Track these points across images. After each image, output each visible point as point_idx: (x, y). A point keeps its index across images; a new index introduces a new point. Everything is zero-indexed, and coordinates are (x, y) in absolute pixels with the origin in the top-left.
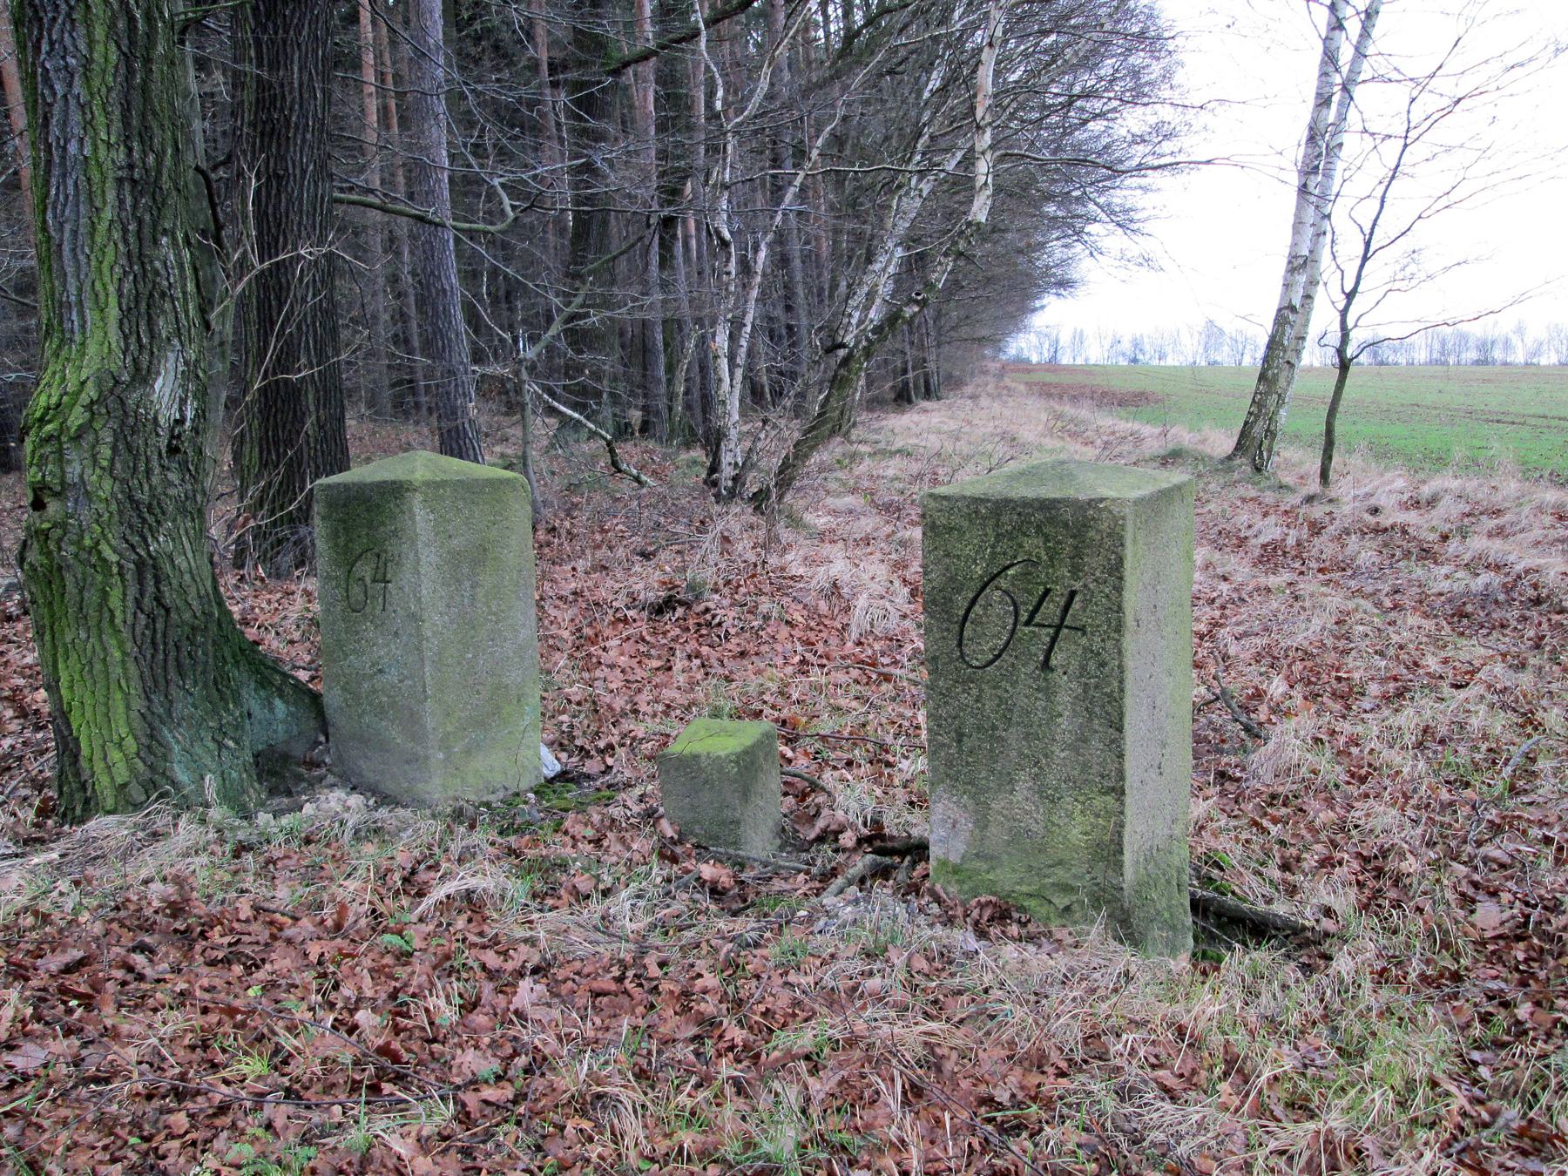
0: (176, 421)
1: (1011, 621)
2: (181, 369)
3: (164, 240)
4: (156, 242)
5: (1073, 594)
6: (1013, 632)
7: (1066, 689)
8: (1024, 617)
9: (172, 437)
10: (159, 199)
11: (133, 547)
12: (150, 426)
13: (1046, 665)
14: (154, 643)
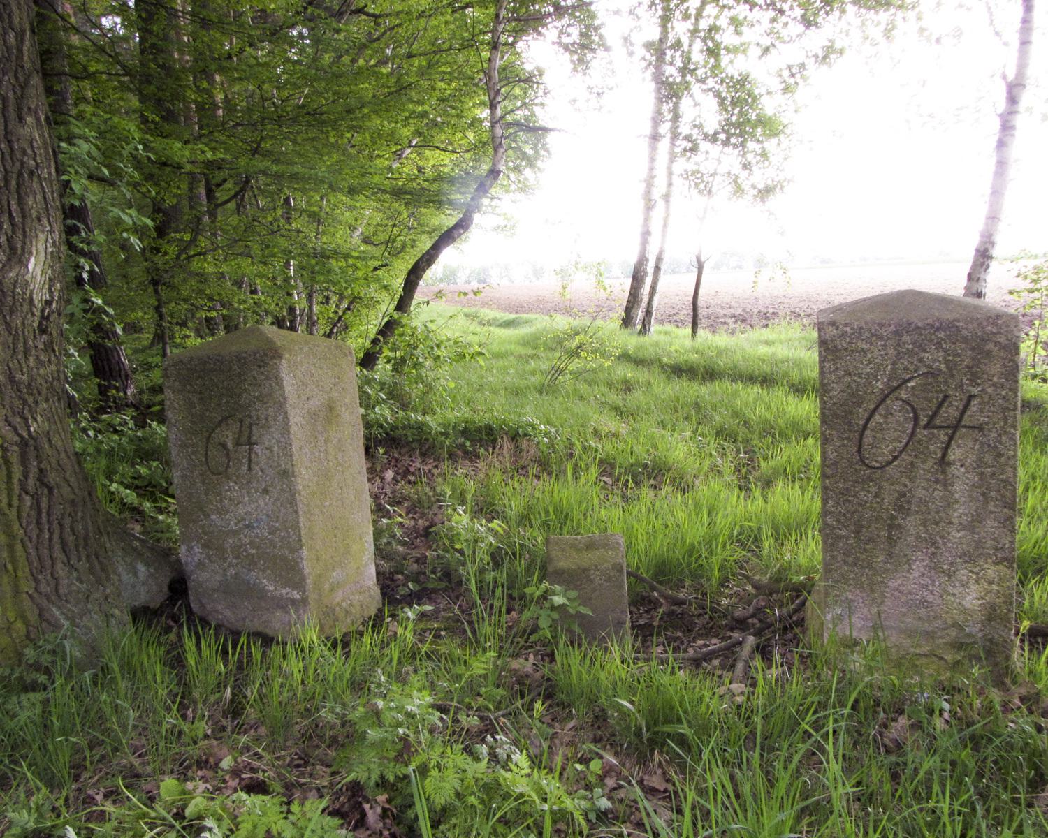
0: (46, 301)
1: (911, 426)
2: (50, 250)
3: (29, 120)
4: (21, 119)
5: (971, 397)
6: (913, 434)
7: (962, 480)
8: (924, 421)
9: (42, 317)
10: (21, 78)
11: (15, 429)
12: (26, 307)
13: (943, 462)
14: (38, 523)
